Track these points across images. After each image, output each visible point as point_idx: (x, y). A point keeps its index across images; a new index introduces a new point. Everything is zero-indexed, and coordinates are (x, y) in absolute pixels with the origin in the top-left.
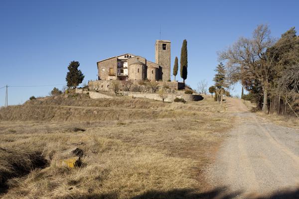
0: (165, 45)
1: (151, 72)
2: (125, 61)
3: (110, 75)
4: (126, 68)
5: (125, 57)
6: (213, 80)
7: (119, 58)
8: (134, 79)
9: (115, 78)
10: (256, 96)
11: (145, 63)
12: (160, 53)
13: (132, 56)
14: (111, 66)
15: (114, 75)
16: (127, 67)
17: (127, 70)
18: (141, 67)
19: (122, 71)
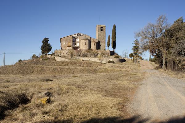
0: (102, 28)
1: (94, 45)
2: (78, 38)
3: (68, 46)
4: (78, 42)
5: (77, 35)
6: (132, 50)
7: (74, 36)
8: (83, 49)
9: (71, 48)
10: (158, 59)
11: (89, 39)
12: (99, 33)
13: (82, 35)
14: (69, 41)
15: (71, 47)
16: (79, 41)
17: (78, 43)
18: (87, 42)
19: (76, 44)
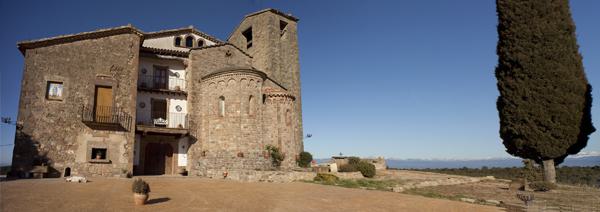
3: (95, 125)
4: (180, 94)
5: (177, 42)
16: (183, 87)
17: (183, 104)
